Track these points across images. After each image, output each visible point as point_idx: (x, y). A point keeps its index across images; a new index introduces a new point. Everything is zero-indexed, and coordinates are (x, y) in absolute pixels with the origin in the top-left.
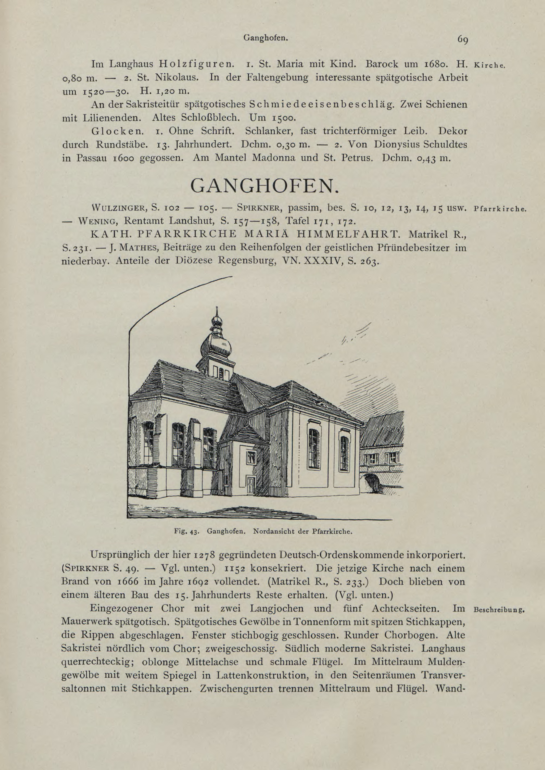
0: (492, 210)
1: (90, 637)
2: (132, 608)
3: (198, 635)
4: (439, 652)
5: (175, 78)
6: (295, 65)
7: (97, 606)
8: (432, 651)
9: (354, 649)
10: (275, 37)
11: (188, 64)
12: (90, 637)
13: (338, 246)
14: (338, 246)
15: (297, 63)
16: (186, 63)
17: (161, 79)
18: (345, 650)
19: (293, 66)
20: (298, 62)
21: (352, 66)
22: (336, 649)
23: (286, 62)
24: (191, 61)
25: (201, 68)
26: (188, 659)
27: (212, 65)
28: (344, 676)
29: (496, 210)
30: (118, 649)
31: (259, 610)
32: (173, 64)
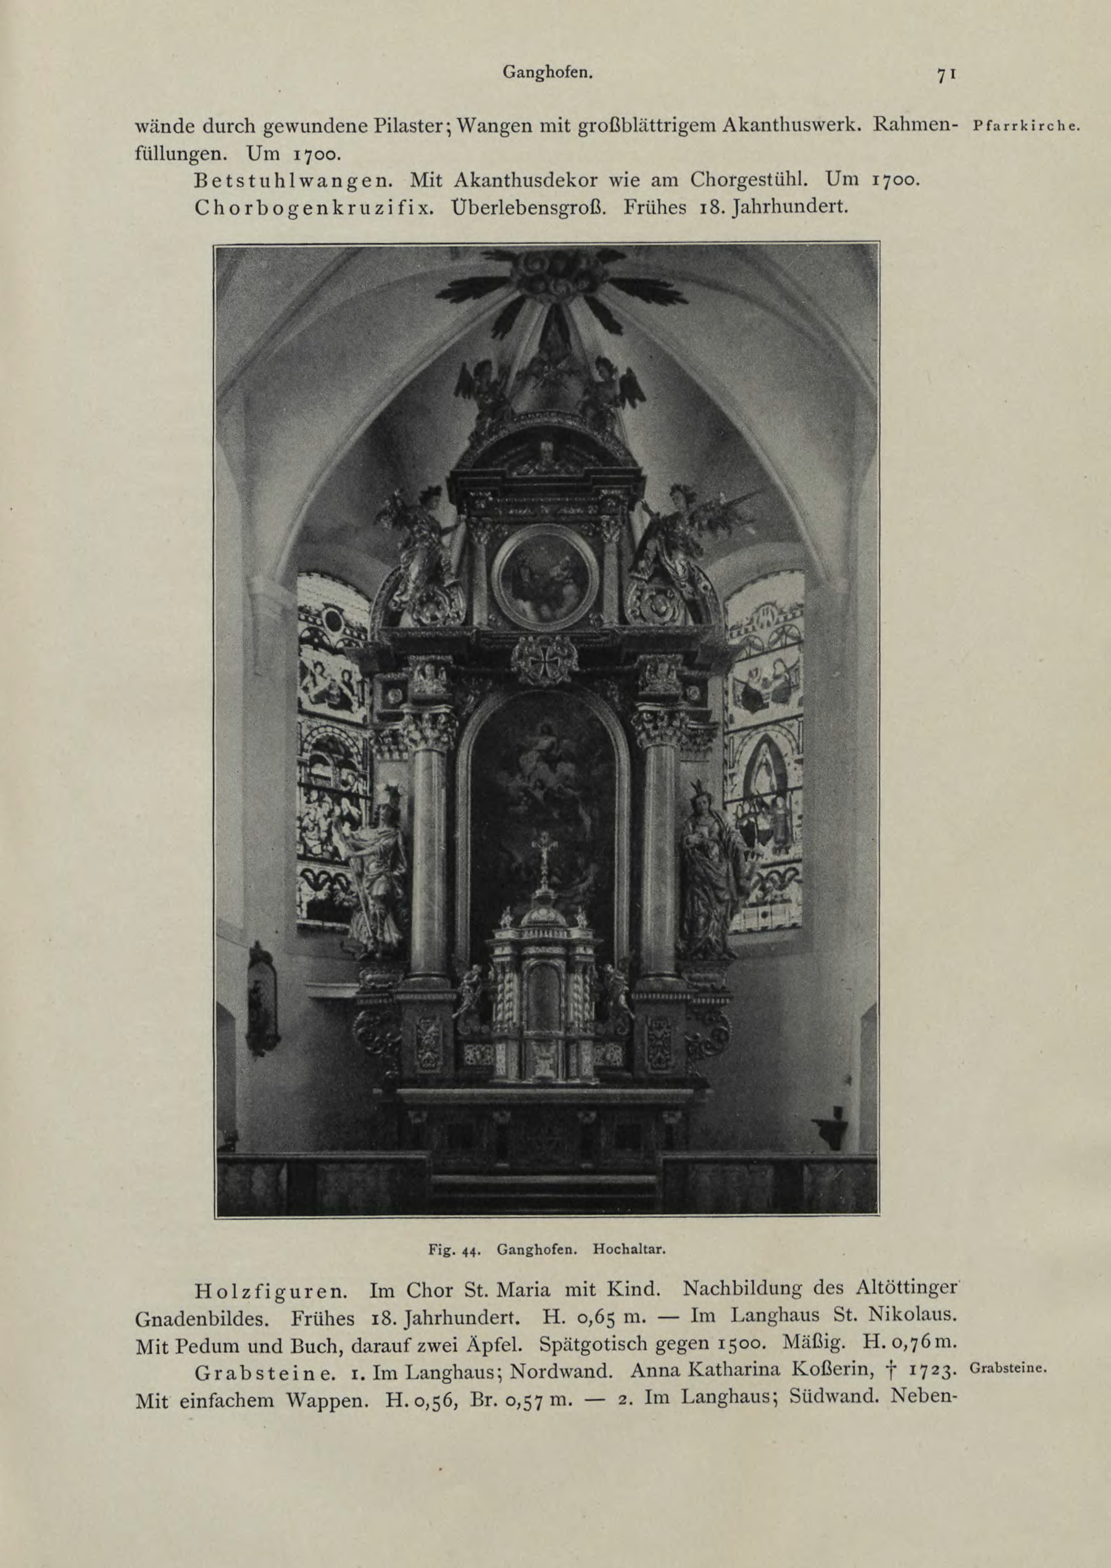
0: (1010, 127)
2: (666, 1344)
5: (909, 1316)
6: (533, 1292)
10: (567, 70)
11: (253, 1293)
15: (537, 1288)
16: (248, 1290)
17: (880, 1318)
19: (529, 1295)
20: (540, 1286)
21: (652, 1294)
23: (514, 1287)
24: (260, 1287)
25: (280, 1300)
26: (787, 1336)
27: (303, 1293)
29: (1018, 127)
31: (424, 1375)
32: (222, 1294)
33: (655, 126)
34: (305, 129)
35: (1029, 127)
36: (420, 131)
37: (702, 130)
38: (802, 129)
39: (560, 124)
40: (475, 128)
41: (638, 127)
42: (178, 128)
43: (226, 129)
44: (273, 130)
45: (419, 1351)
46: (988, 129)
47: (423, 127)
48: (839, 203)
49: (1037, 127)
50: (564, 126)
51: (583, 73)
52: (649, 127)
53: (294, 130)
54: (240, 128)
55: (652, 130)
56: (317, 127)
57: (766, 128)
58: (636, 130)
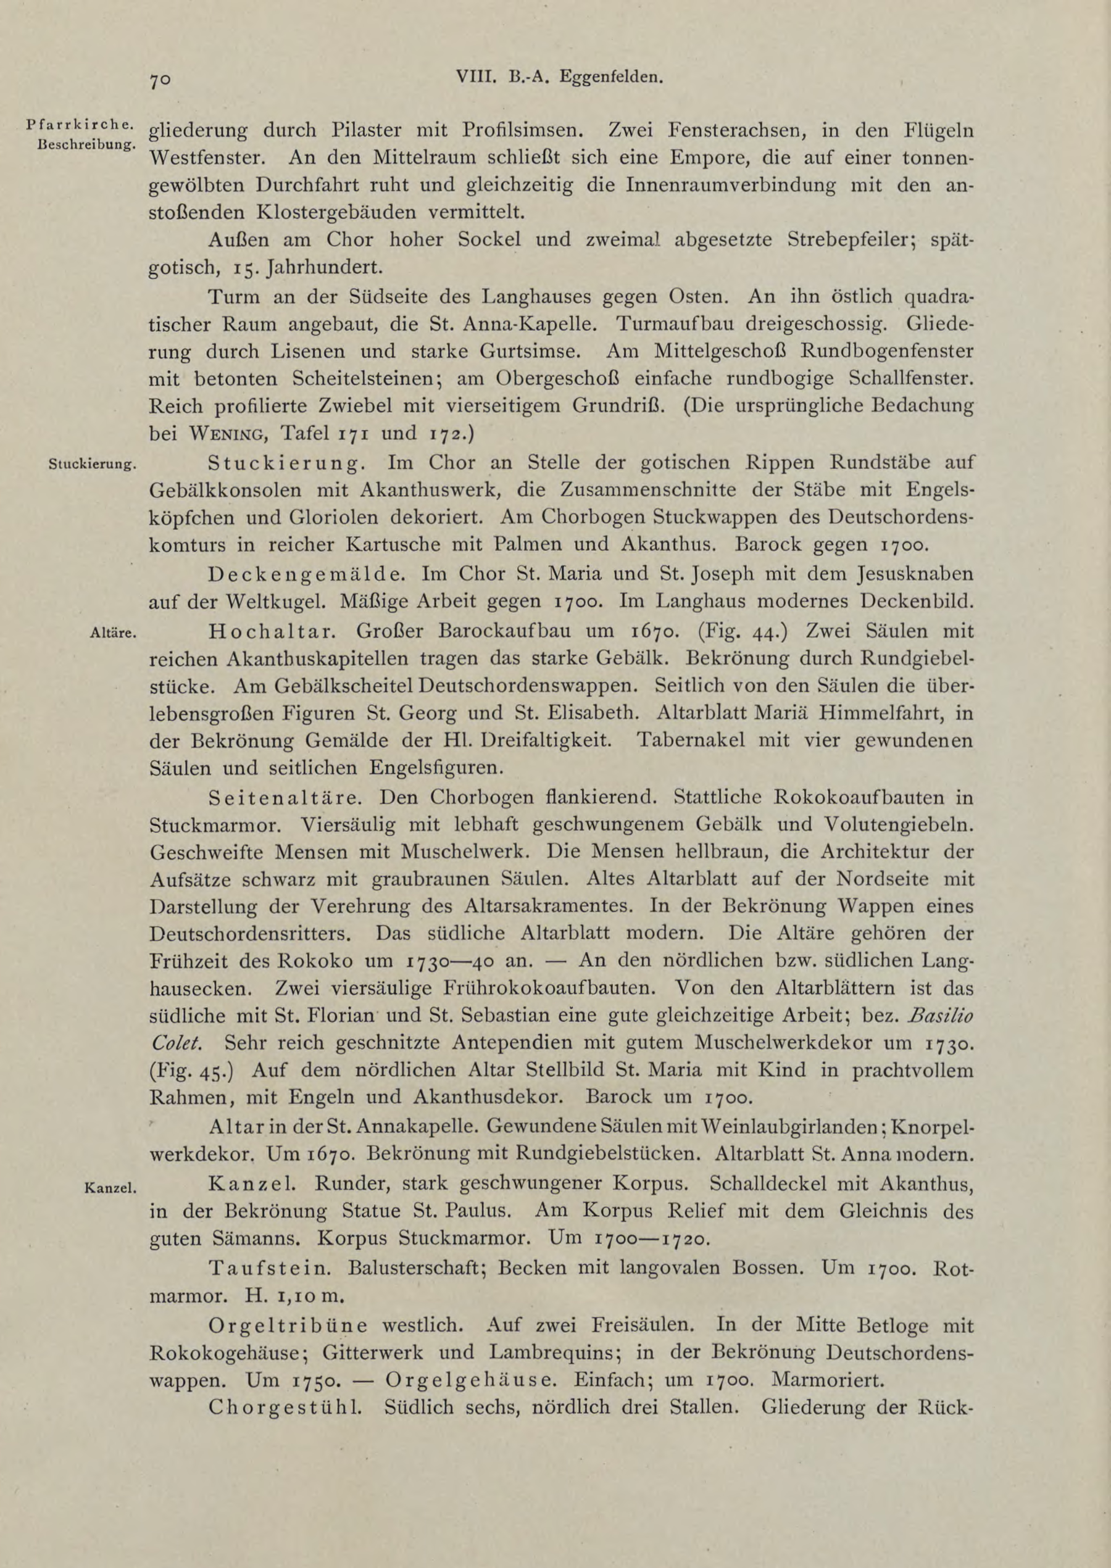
0: (63, 126)
1: (765, 468)
3: (680, 129)
4: (815, 912)
7: (589, 1375)
8: (294, 884)
9: (686, 934)
12: (765, 468)
13: (630, 1321)
14: (630, 1321)
18: (927, 744)
22: (650, 934)
28: (355, 159)
30: (688, 960)
33: (857, 989)
34: (605, 827)
35: (83, 126)
36: (951, 356)
37: (335, 746)
38: (725, 1046)
39: (267, 1096)
40: (856, 908)
41: (840, 989)
42: (216, 214)
43: (287, 133)
44: (345, 1046)
45: (588, 245)
46: (41, 128)
47: (949, 380)
48: (474, 514)
49: (91, 126)
50: (501, 1153)
51: (653, 77)
52: (850, 989)
53: (594, 828)
54: (837, 660)
55: (736, 717)
56: (462, 880)
57: (457, 1099)
58: (838, 993)
